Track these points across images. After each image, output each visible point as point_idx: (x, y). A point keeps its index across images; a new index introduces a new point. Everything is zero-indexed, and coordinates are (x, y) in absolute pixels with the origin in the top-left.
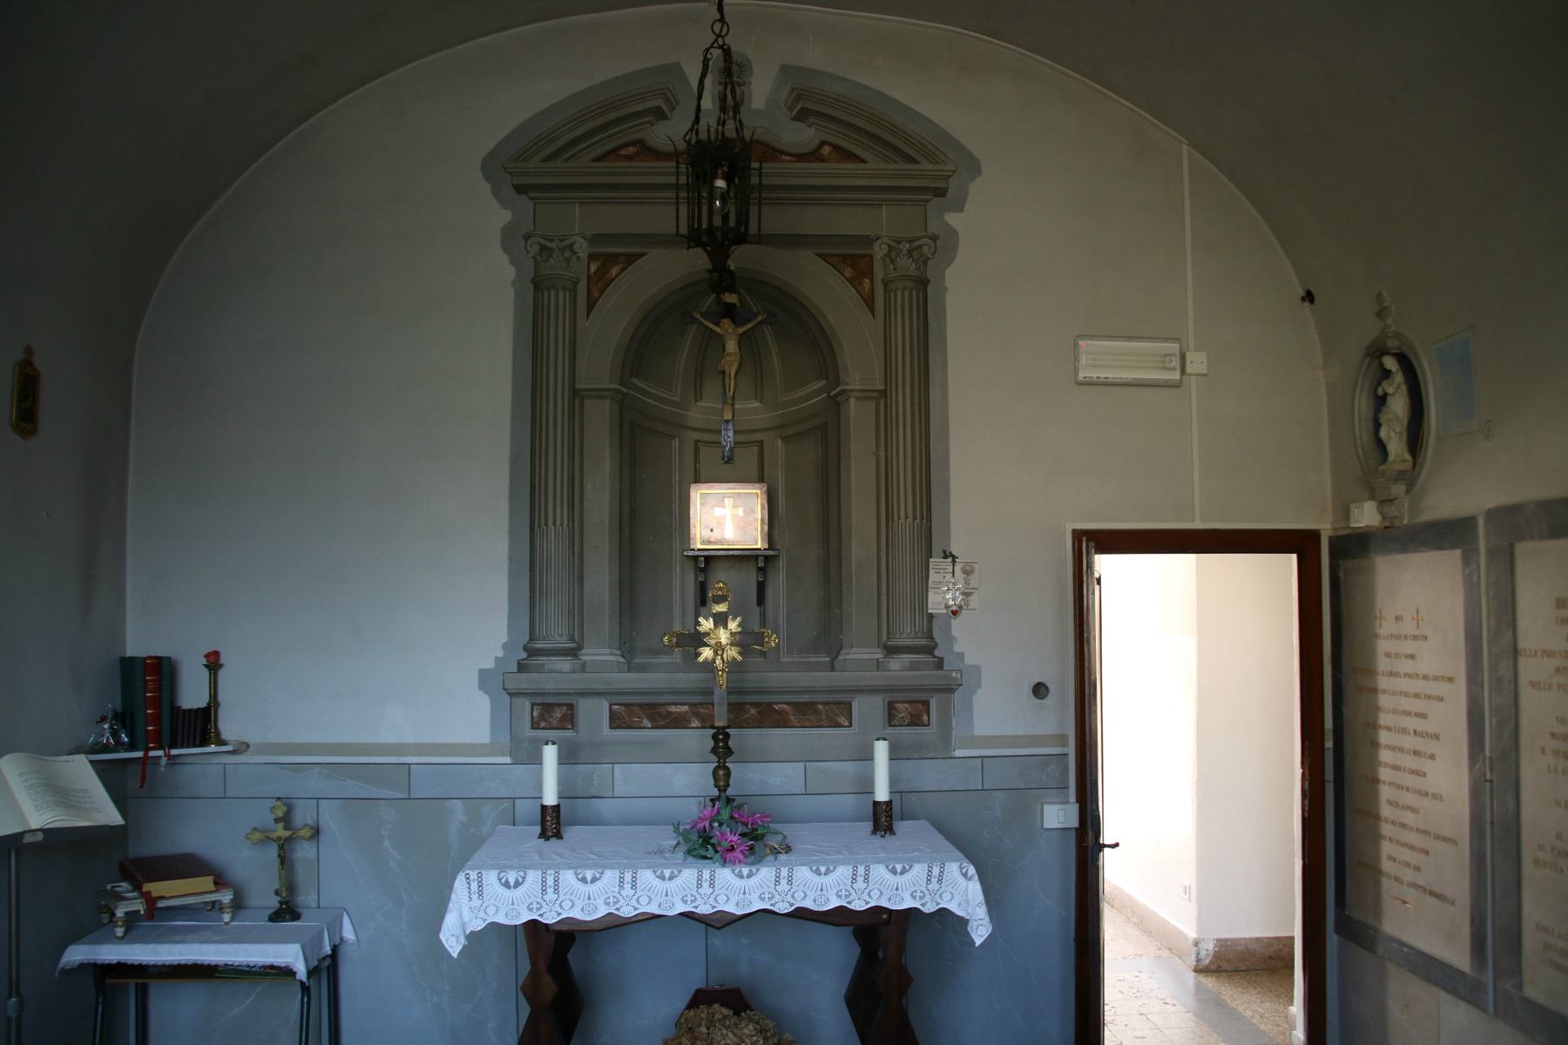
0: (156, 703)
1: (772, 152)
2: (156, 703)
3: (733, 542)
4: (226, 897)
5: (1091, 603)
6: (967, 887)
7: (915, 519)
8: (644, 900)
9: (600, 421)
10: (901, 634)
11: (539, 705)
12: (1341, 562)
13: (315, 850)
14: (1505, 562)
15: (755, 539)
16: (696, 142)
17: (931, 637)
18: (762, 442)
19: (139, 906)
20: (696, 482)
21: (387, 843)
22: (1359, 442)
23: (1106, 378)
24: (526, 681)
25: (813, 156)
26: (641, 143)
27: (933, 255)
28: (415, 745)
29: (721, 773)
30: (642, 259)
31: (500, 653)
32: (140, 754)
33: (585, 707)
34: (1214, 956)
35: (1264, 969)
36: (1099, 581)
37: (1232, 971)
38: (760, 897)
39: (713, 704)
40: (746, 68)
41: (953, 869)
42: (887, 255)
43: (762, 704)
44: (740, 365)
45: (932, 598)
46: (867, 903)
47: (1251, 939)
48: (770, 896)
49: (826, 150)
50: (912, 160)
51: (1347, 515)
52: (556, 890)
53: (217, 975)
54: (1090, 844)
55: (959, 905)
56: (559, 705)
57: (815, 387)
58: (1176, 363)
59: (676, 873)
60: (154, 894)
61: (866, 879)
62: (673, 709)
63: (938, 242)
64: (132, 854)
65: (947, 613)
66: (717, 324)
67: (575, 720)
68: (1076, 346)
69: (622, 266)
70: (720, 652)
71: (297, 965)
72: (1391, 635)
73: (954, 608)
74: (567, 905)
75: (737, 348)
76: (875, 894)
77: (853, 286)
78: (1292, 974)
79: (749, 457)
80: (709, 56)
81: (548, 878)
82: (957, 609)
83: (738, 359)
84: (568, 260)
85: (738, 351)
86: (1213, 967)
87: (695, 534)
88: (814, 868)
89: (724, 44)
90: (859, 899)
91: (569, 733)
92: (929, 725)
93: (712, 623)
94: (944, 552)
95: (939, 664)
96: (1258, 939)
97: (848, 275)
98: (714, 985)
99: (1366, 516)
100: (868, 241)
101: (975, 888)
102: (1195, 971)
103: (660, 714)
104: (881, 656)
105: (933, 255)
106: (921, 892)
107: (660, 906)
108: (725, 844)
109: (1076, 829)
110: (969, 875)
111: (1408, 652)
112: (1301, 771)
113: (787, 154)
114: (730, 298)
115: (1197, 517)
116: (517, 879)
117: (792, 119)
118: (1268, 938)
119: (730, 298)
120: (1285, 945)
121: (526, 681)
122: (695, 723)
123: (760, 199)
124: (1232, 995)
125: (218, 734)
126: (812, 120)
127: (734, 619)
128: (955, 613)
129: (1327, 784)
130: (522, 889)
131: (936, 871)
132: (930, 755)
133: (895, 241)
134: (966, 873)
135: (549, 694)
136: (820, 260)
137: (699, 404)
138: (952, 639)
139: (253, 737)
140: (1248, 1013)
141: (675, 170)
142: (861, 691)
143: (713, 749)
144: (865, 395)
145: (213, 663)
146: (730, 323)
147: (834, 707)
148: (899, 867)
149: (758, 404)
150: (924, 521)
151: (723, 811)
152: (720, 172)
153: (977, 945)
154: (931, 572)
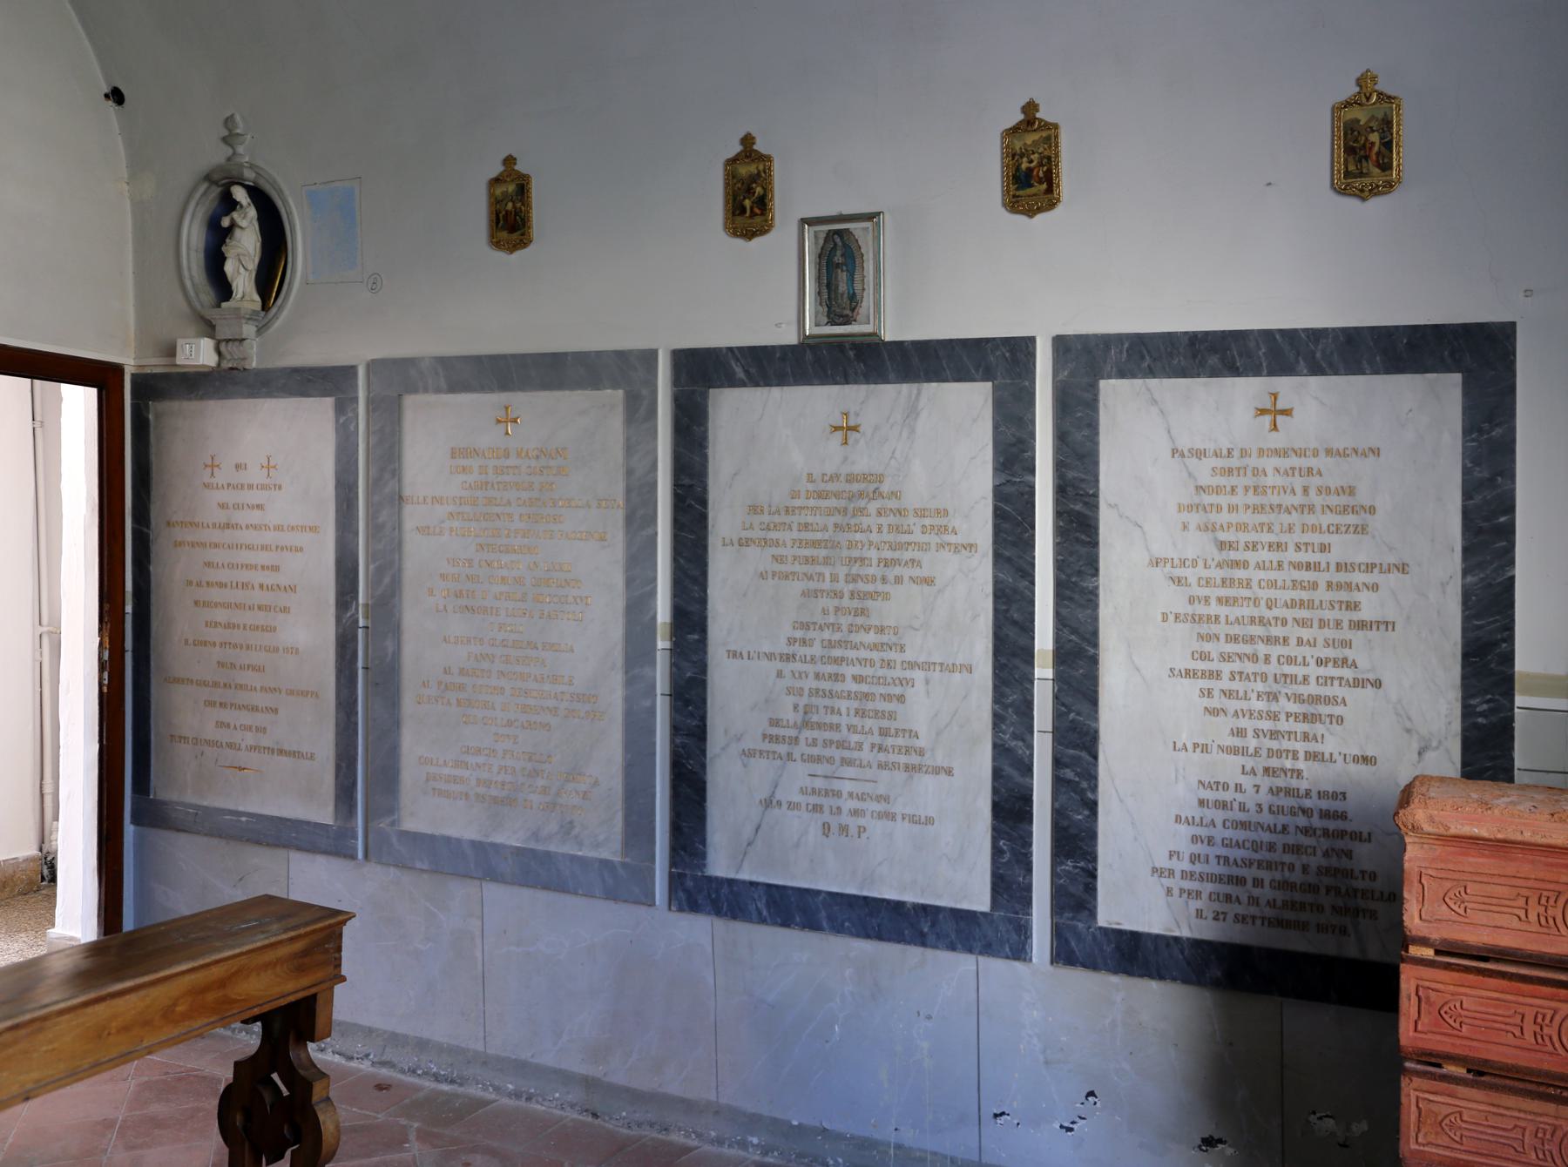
12: (150, 403)
14: (388, 413)
72: (229, 485)
99: (200, 354)
111: (256, 502)
112: (99, 639)
129: (126, 654)
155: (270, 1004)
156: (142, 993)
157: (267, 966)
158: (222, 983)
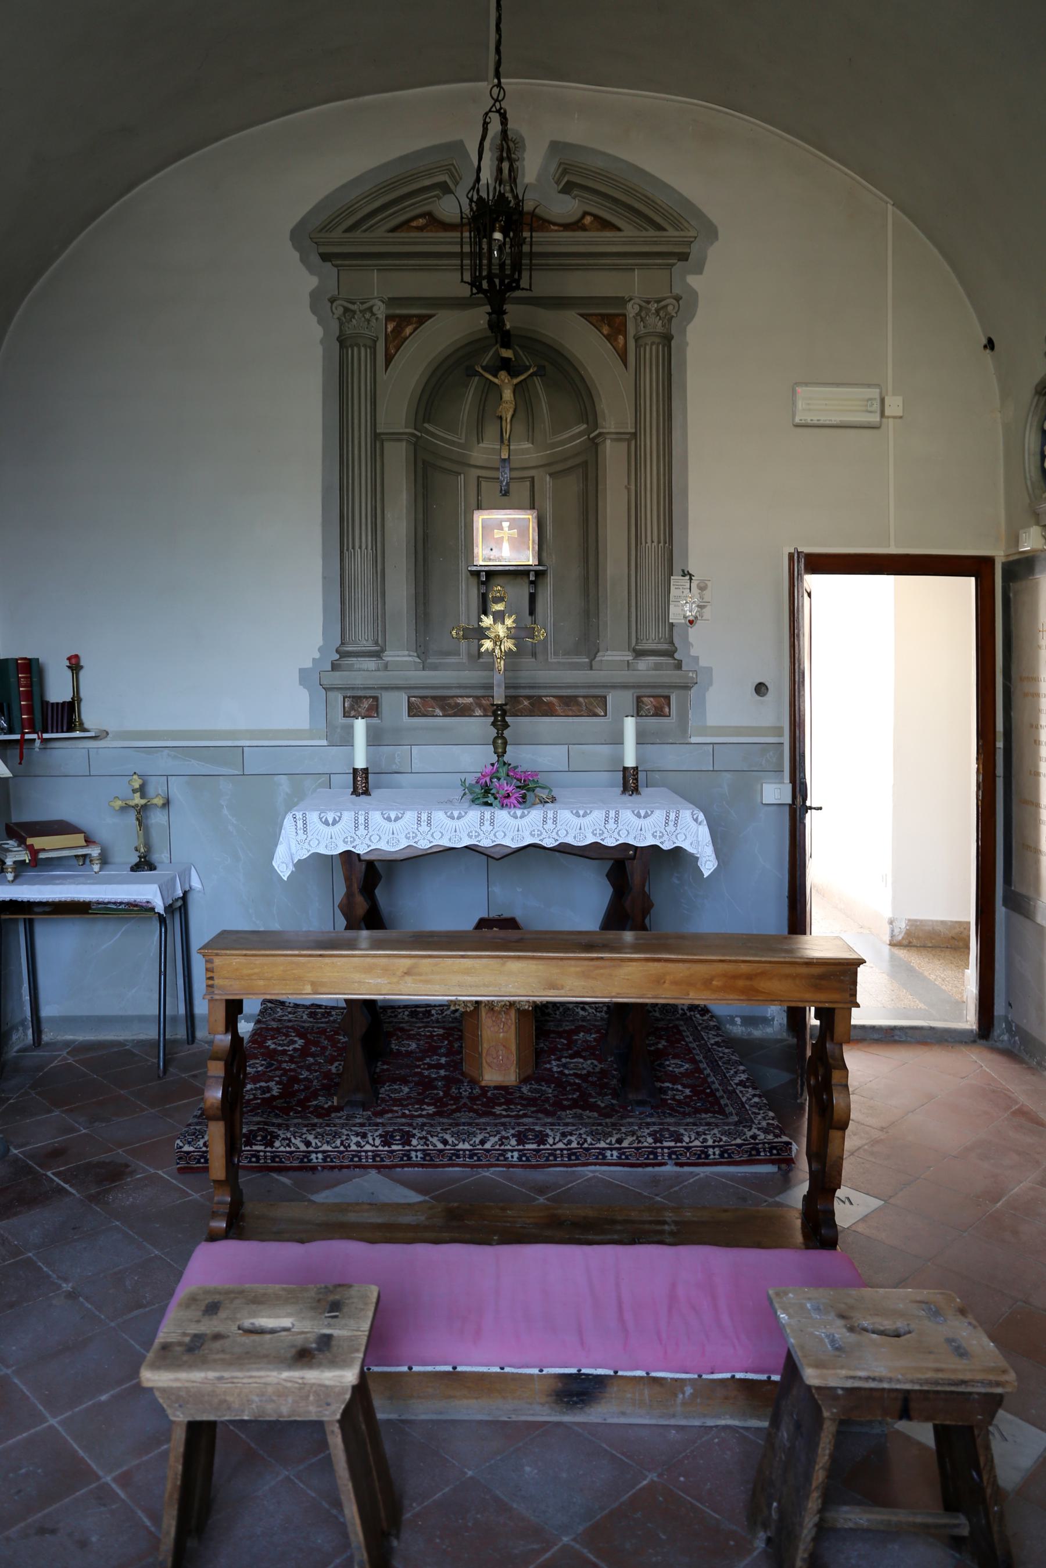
0: (29, 695)
1: (541, 223)
2: (29, 695)
3: (509, 559)
4: (95, 852)
5: (800, 604)
6: (698, 830)
7: (659, 542)
8: (437, 835)
9: (397, 456)
10: (647, 640)
11: (349, 697)
12: (1011, 584)
13: (167, 817)
15: (528, 558)
16: (478, 199)
17: (672, 643)
18: (533, 478)
19: (26, 857)
20: (478, 509)
21: (225, 811)
22: (1028, 476)
23: (818, 420)
24: (338, 678)
25: (576, 226)
26: (429, 215)
27: (676, 313)
28: (247, 731)
29: (500, 741)
30: (432, 319)
31: (317, 655)
32: (18, 737)
33: (387, 700)
34: (906, 933)
35: (947, 948)
36: (809, 595)
37: (920, 947)
38: (531, 834)
39: (493, 697)
40: (520, 143)
41: (686, 815)
42: (637, 314)
43: (532, 697)
44: (515, 411)
45: (673, 609)
46: (617, 840)
47: (937, 921)
48: (539, 833)
49: (588, 220)
50: (661, 228)
51: (1016, 540)
52: (366, 827)
53: (90, 911)
54: (799, 806)
55: (691, 844)
56: (366, 698)
57: (577, 431)
58: (876, 406)
59: (463, 814)
60: (36, 847)
61: (616, 821)
62: (460, 701)
63: (680, 302)
64: (15, 819)
65: (685, 623)
66: (495, 376)
67: (380, 709)
68: (794, 393)
69: (414, 326)
70: (498, 643)
71: (156, 901)
73: (691, 618)
74: (375, 838)
75: (512, 396)
76: (624, 833)
77: (609, 342)
78: (969, 953)
79: (522, 490)
80: (488, 120)
81: (360, 817)
82: (693, 619)
83: (513, 406)
84: (368, 321)
85: (513, 399)
86: (905, 942)
87: (478, 553)
88: (574, 812)
89: (501, 108)
90: (611, 837)
91: (375, 721)
92: (669, 716)
93: (492, 619)
94: (683, 571)
95: (679, 666)
96: (942, 922)
97: (605, 332)
98: (493, 915)
100: (622, 301)
101: (704, 831)
102: (890, 945)
103: (449, 705)
104: (631, 658)
105: (676, 313)
106: (661, 832)
107: (450, 839)
108: (502, 792)
109: (790, 805)
110: (699, 821)
112: (976, 766)
113: (555, 224)
114: (507, 353)
115: (892, 543)
116: (334, 818)
117: (559, 192)
118: (951, 922)
119: (507, 353)
120: (965, 929)
121: (338, 678)
122: (478, 712)
123: (531, 265)
124: (920, 964)
125: (81, 724)
126: (575, 192)
127: (510, 616)
128: (691, 622)
129: (997, 779)
130: (338, 826)
131: (672, 816)
132: (671, 741)
133: (644, 301)
134: (697, 818)
135: (358, 688)
136: (582, 319)
137: (481, 445)
138: (688, 645)
139: (111, 726)
140: (932, 977)
141: (459, 240)
142: (614, 687)
143: (492, 722)
144: (619, 437)
145: (75, 665)
146: (506, 374)
147: (591, 699)
148: (642, 813)
149: (530, 445)
150: (667, 545)
151: (500, 770)
152: (497, 225)
153: (705, 877)
154: (672, 588)
155: (790, 1003)
156: (687, 965)
157: (787, 976)
158: (749, 977)
